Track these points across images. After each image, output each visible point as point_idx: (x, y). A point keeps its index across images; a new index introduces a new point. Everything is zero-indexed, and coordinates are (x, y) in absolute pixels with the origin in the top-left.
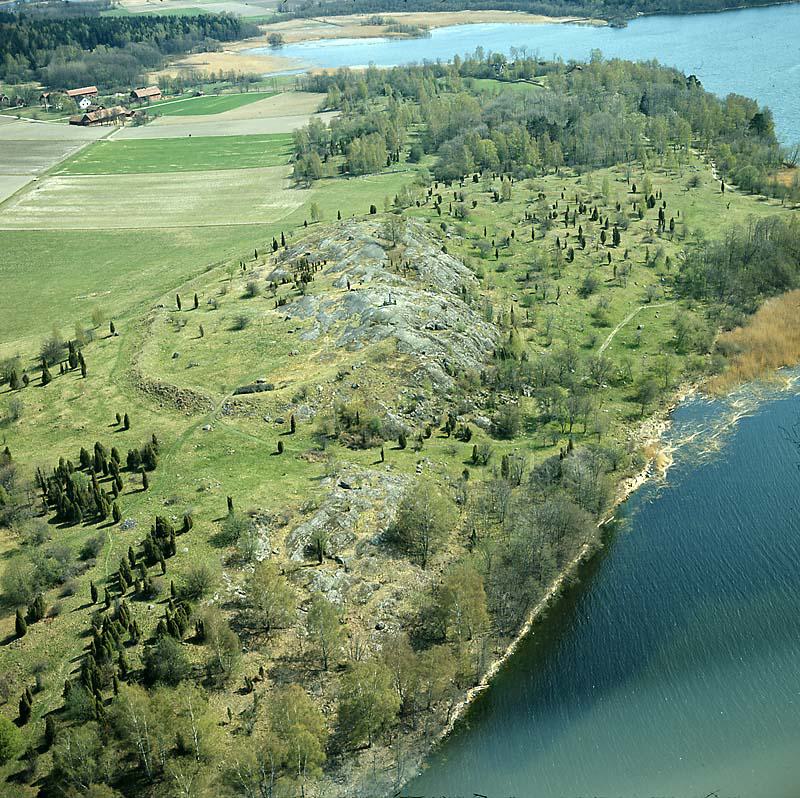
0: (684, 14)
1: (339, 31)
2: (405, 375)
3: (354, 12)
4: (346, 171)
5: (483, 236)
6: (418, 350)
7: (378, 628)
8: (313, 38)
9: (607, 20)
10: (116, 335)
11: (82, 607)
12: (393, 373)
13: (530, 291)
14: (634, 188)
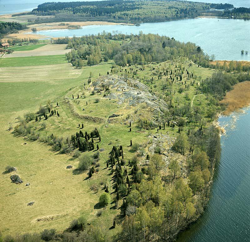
0: (155, 22)
1: (50, 27)
2: (151, 112)
3: (54, 22)
4: (89, 64)
5: (144, 79)
6: (152, 105)
7: (181, 169)
8: (45, 29)
9: (134, 24)
10: (59, 106)
11: (104, 169)
12: (148, 111)
13: (166, 92)
14: (176, 66)
